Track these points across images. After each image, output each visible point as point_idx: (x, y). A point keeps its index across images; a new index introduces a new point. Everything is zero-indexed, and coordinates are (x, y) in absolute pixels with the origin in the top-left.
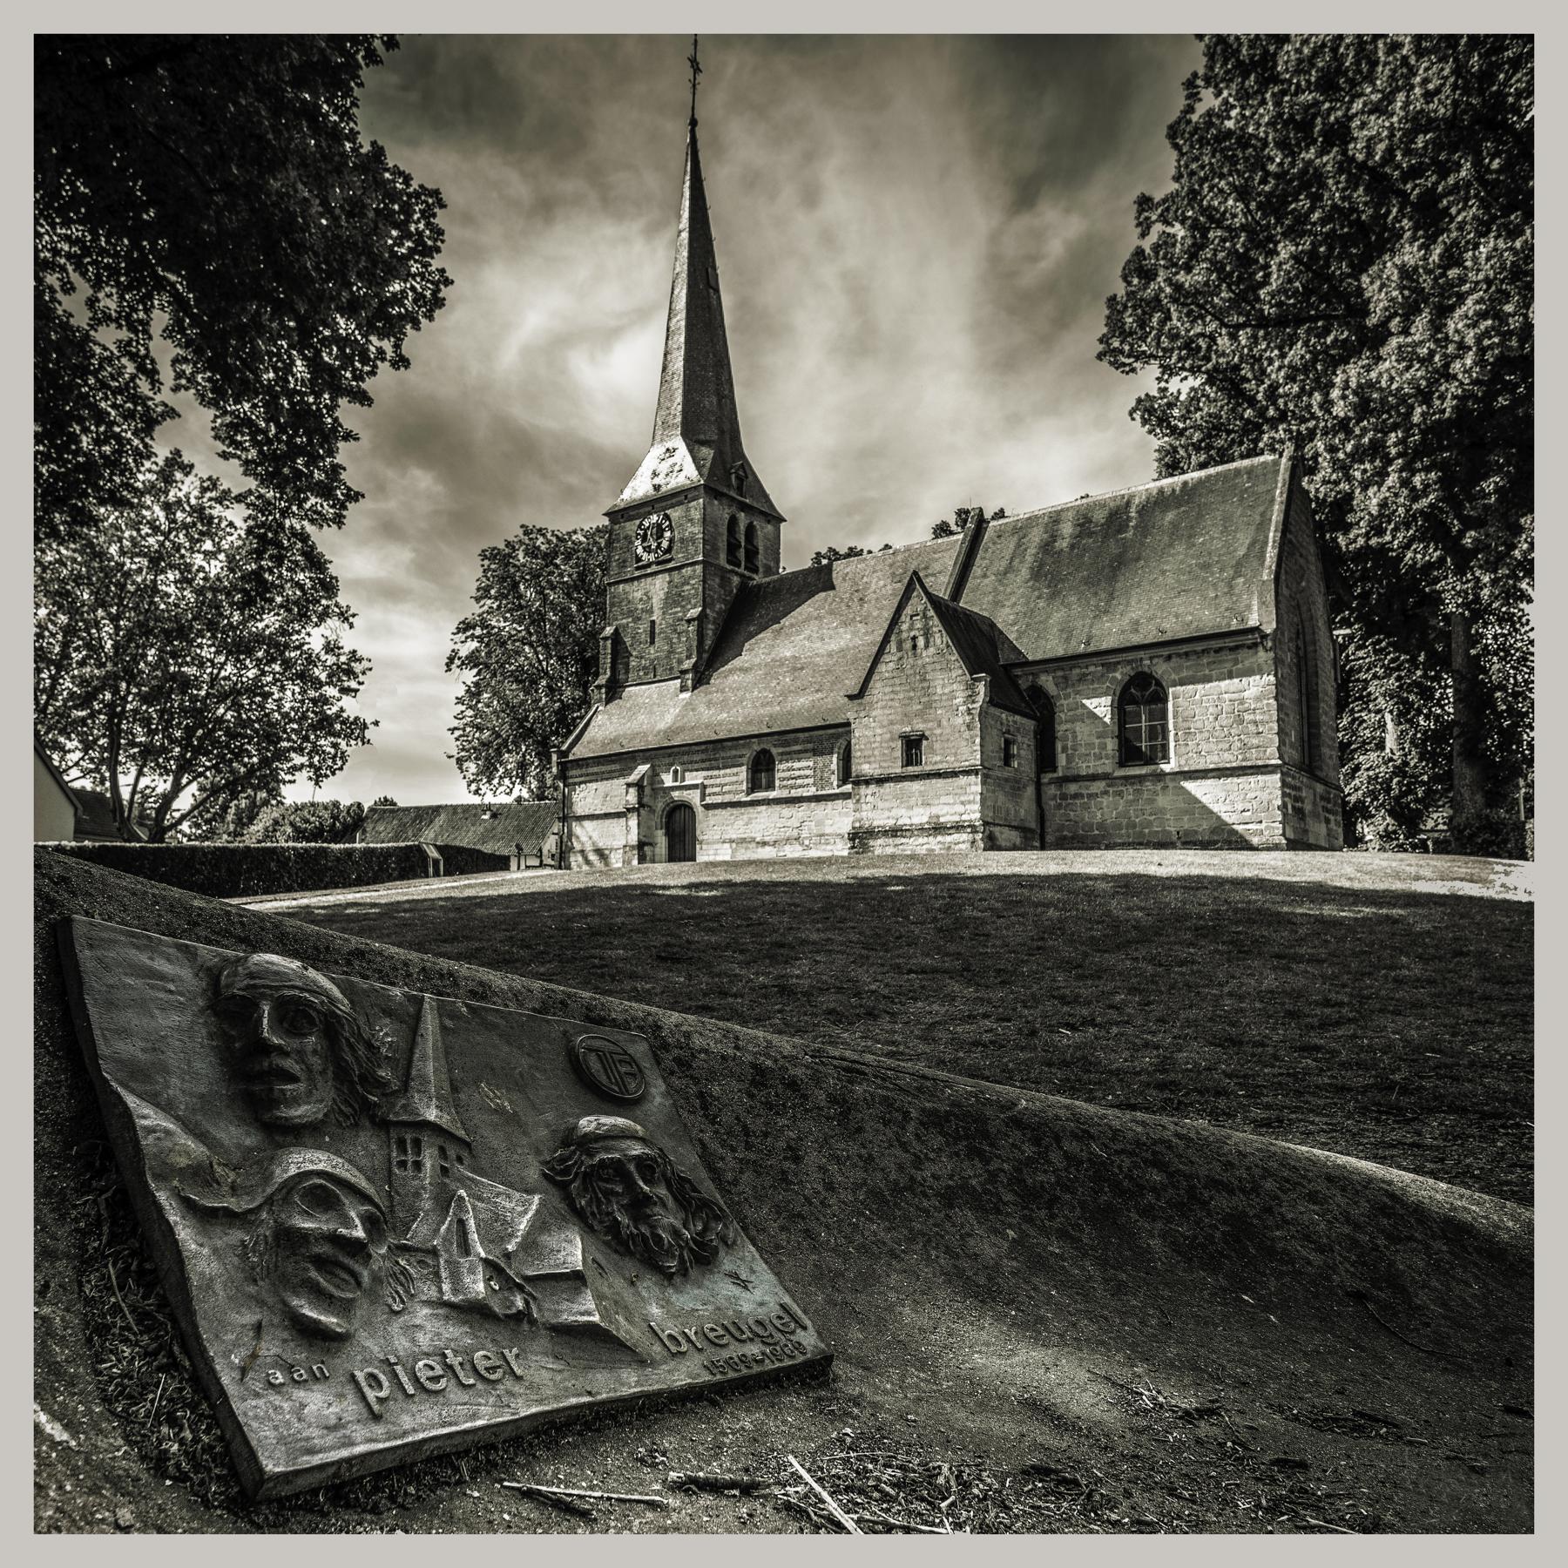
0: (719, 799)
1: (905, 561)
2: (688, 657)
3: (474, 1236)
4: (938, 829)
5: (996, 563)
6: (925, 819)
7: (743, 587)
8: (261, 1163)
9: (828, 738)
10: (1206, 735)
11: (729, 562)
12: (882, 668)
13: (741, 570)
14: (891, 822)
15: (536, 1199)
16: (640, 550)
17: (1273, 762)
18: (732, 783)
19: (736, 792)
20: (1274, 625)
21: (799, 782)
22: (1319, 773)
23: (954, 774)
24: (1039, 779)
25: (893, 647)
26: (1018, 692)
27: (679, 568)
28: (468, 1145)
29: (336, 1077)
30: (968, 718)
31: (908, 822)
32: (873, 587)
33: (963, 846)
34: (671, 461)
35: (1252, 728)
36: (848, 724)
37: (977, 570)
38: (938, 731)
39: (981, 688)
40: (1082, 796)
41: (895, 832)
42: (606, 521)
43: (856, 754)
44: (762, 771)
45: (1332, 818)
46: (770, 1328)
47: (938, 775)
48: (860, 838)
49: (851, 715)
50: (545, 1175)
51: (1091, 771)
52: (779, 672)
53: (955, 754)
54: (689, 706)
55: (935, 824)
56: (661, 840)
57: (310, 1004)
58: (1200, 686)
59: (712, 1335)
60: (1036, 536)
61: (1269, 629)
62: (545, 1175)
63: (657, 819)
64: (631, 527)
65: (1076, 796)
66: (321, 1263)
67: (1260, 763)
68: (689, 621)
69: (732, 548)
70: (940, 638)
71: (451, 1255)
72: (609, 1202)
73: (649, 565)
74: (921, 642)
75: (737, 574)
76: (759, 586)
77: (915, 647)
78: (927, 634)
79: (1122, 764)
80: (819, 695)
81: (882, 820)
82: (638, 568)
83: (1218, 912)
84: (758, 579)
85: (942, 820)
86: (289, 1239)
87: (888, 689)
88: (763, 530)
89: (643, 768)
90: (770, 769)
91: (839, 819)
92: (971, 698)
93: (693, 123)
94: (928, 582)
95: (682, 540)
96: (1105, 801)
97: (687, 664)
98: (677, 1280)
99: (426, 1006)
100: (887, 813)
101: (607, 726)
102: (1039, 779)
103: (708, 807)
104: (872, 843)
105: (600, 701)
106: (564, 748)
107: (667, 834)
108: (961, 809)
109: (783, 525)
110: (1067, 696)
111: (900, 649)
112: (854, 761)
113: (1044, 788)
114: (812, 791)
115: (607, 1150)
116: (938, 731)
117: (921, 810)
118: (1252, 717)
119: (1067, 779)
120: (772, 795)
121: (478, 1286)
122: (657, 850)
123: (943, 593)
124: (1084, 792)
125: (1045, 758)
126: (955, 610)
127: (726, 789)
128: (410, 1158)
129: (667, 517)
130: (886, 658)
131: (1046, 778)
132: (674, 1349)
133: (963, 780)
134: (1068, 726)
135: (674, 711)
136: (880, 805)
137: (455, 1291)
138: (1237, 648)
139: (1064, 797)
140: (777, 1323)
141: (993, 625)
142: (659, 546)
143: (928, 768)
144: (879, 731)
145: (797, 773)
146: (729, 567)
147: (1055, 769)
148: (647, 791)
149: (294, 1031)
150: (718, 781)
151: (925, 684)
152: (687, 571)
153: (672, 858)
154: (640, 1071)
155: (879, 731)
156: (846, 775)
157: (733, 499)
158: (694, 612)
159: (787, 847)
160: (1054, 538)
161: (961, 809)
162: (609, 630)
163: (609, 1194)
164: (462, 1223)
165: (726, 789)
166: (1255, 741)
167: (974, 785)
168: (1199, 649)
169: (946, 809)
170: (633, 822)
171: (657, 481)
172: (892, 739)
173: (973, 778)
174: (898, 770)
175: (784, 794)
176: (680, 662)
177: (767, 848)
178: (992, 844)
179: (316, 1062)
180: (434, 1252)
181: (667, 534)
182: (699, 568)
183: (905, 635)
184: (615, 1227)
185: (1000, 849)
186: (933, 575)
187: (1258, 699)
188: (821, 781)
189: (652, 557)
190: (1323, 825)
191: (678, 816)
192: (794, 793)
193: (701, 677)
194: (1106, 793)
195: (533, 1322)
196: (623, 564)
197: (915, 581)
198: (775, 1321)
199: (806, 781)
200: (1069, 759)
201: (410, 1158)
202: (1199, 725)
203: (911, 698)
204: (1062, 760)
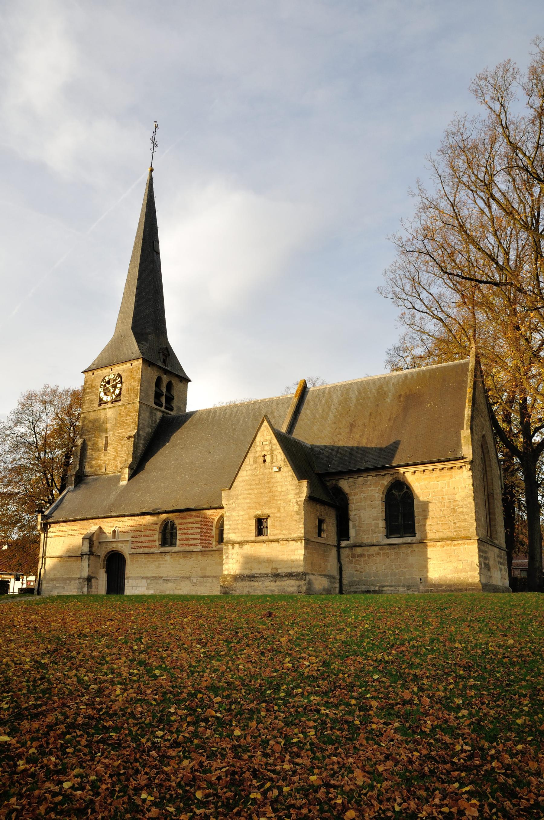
7: (163, 419)
20: (471, 457)
21: (192, 542)
22: (496, 542)
24: (339, 544)
38: (278, 515)
45: (502, 567)
47: (277, 541)
58: (506, 567)
60: (337, 398)
63: (101, 561)
65: (361, 556)
69: (158, 395)
70: (280, 455)
74: (268, 459)
75: (160, 410)
77: (264, 461)
78: (272, 451)
79: (388, 536)
87: (247, 487)
88: (177, 385)
90: (173, 535)
92: (299, 494)
93: (152, 170)
96: (378, 559)
102: (339, 544)
107: (107, 572)
109: (189, 383)
110: (356, 494)
111: (255, 461)
112: (225, 532)
113: (342, 551)
114: (199, 548)
116: (278, 515)
118: (461, 510)
119: (355, 546)
123: (284, 429)
124: (366, 553)
125: (343, 532)
126: (290, 439)
131: (344, 544)
139: (354, 556)
143: (271, 538)
145: (190, 536)
146: (155, 407)
147: (348, 539)
148: (96, 543)
151: (271, 485)
170: (85, 563)
174: (253, 538)
175: (182, 549)
177: (170, 584)
187: (463, 500)
190: (499, 572)
192: (188, 548)
194: (378, 554)
200: (357, 534)
204: (352, 533)
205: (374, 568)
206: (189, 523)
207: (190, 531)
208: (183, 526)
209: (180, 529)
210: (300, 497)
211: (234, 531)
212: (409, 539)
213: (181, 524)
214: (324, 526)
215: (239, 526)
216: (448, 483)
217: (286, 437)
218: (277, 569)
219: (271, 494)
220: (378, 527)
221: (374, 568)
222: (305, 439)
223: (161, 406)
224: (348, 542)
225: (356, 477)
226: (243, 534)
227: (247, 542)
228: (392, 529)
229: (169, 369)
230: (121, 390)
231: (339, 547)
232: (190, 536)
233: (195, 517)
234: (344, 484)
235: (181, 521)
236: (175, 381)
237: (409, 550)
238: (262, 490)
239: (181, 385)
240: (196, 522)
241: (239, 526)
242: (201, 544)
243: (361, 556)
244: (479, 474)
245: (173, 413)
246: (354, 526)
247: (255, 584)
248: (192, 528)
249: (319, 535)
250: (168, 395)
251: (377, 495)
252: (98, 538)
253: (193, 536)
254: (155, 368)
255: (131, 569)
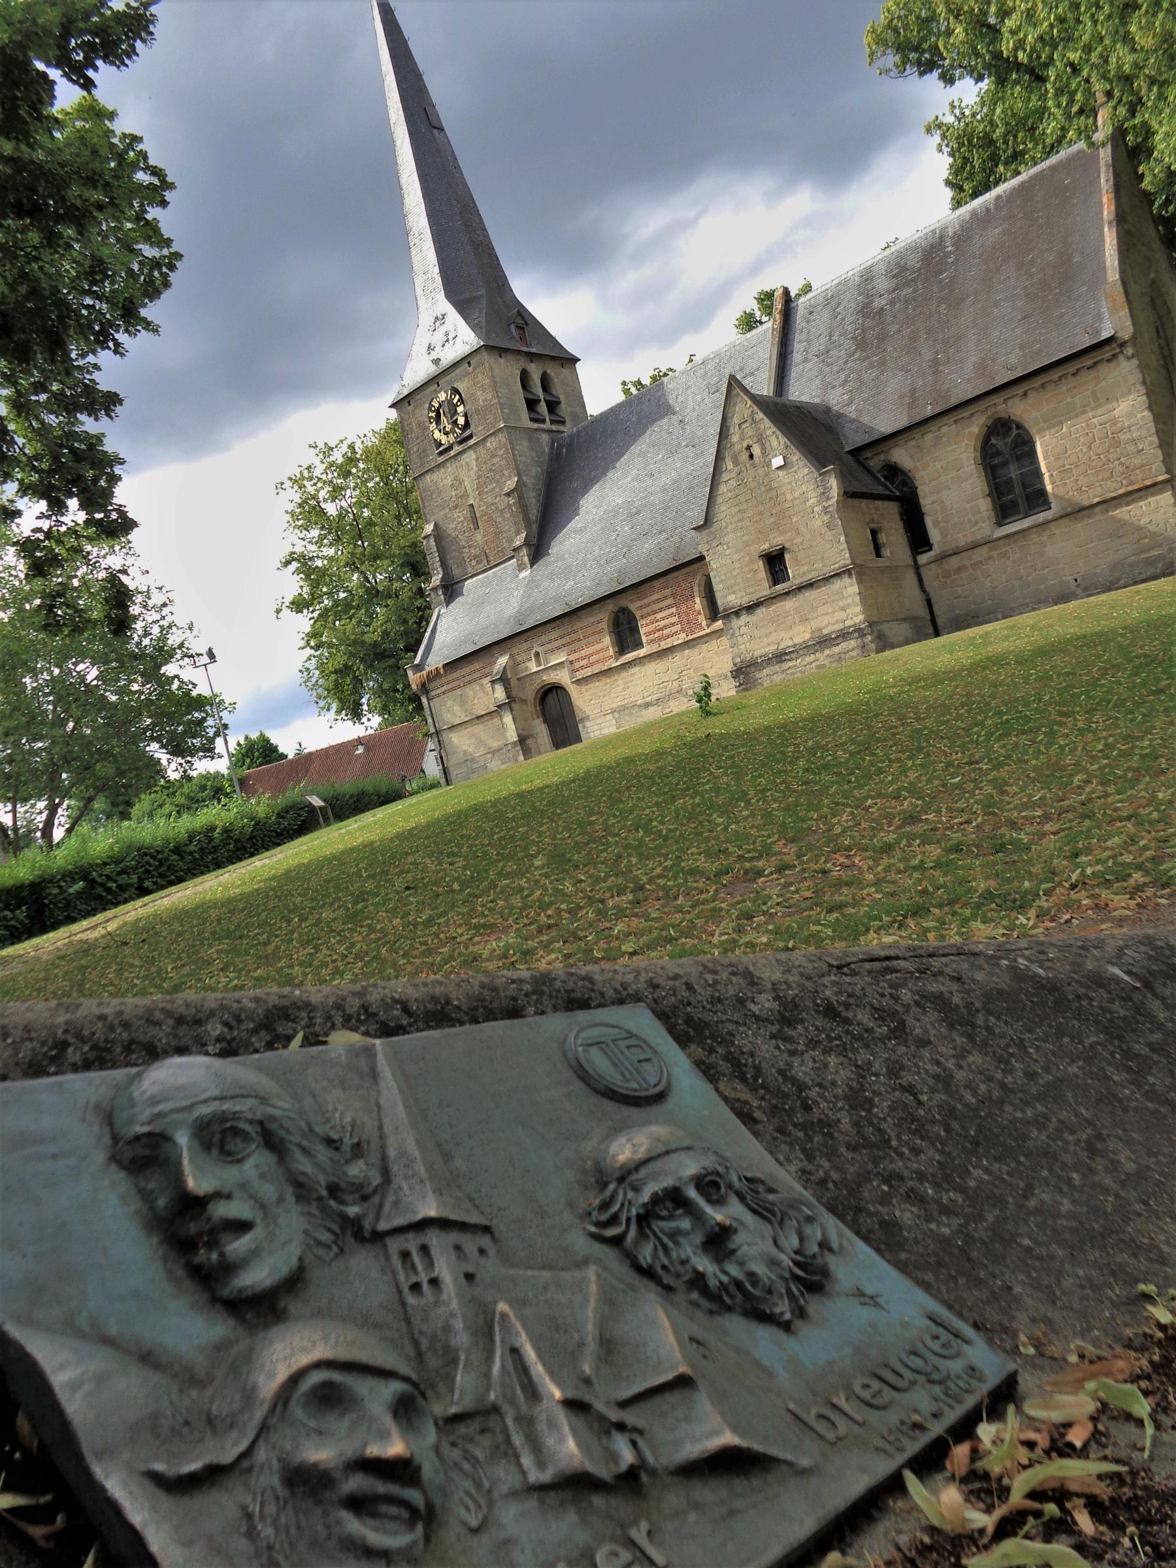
0: (588, 672)
1: (718, 367)
2: (518, 533)
3: (538, 1369)
4: (823, 642)
5: (815, 344)
6: (807, 636)
8: (237, 1365)
9: (686, 573)
10: (1083, 468)
11: (532, 420)
12: (723, 488)
13: (547, 425)
14: (773, 648)
15: (591, 1273)
16: (437, 435)
17: (1161, 478)
18: (598, 652)
19: (605, 660)
20: (1131, 329)
23: (827, 580)
24: (915, 561)
25: (729, 464)
26: (875, 478)
27: (484, 440)
28: (487, 1229)
29: (299, 1198)
30: (826, 518)
31: (790, 643)
32: (691, 404)
33: (854, 653)
34: (442, 330)
35: (1131, 448)
36: (702, 558)
37: (797, 356)
38: (799, 540)
39: (833, 483)
40: (965, 568)
41: (780, 657)
42: (393, 414)
43: (717, 587)
44: (625, 634)
46: (929, 1355)
47: (810, 585)
48: (743, 673)
49: (703, 549)
50: (593, 1236)
51: (969, 539)
52: (611, 526)
53: (822, 559)
54: (531, 583)
55: (814, 638)
56: (541, 730)
57: (235, 1116)
59: (866, 1395)
61: (1126, 332)
62: (593, 1236)
63: (531, 708)
64: (423, 413)
65: (959, 570)
66: (358, 1504)
67: (1148, 483)
68: (508, 494)
69: (531, 404)
70: (777, 440)
71: (518, 1409)
72: (677, 1243)
73: (450, 448)
74: (756, 450)
76: (571, 437)
77: (751, 456)
78: (761, 439)
79: (1000, 524)
80: (664, 536)
81: (763, 648)
82: (441, 453)
83: (106, 599)
84: (567, 429)
85: (825, 632)
86: (305, 1482)
87: (735, 510)
88: (558, 375)
89: (503, 661)
90: (635, 630)
91: (716, 660)
92: (825, 495)
94: (747, 383)
95: (477, 411)
97: (519, 540)
98: (798, 1323)
99: (380, 1057)
100: (766, 641)
101: (451, 630)
102: (915, 561)
103: (578, 682)
104: (758, 675)
105: (439, 604)
106: (417, 661)
107: (545, 721)
108: (843, 615)
109: (578, 365)
111: (736, 463)
113: (923, 571)
114: (682, 638)
115: (654, 1176)
116: (799, 540)
117: (801, 628)
118: (1128, 436)
119: (944, 557)
120: (642, 652)
121: (568, 1448)
122: (540, 740)
125: (919, 540)
126: (785, 406)
127: (593, 659)
128: (424, 1278)
129: (456, 391)
130: (725, 477)
131: (923, 559)
132: (831, 1436)
133: (837, 584)
134: (934, 498)
135: (518, 594)
136: (756, 633)
137: (541, 1465)
138: (1095, 364)
139: (947, 574)
140: (936, 1346)
141: (827, 410)
142: (455, 423)
144: (736, 557)
145: (662, 623)
146: (535, 426)
148: (513, 682)
149: (229, 1156)
150: (583, 653)
151: (773, 493)
152: (491, 444)
153: (558, 744)
154: (655, 1052)
155: (736, 557)
156: (714, 612)
157: (519, 352)
158: (511, 483)
159: (671, 703)
160: (870, 298)
161: (843, 615)
162: (429, 528)
163: (674, 1235)
164: (515, 1351)
165: (593, 659)
166: (1137, 461)
167: (850, 588)
168: (1089, 363)
169: (826, 619)
170: (508, 719)
171: (434, 355)
172: (752, 561)
173: (846, 580)
174: (767, 592)
175: (655, 648)
176: (511, 541)
177: (652, 709)
178: (884, 643)
179: (268, 1191)
180: (495, 1409)
181: (460, 409)
182: (502, 437)
183: (737, 447)
184: (698, 1281)
185: (892, 646)
186: (752, 374)
187: (1130, 415)
188: (689, 624)
189: (452, 438)
191: (551, 698)
192: (664, 645)
193: (537, 549)
194: (990, 558)
195: (653, 1473)
196: (423, 454)
197: (734, 384)
198: (929, 1343)
199: (673, 629)
201: (424, 1278)
202: (1073, 459)
203: (761, 513)
204: (934, 535)
205: (988, 584)
206: (654, 602)
207: (659, 616)
208: (645, 611)
209: (642, 617)
210: (828, 499)
211: (731, 589)
212: (1042, 517)
213: (641, 607)
214: (882, 538)
215: (739, 580)
216: (1094, 394)
217: (776, 404)
218: (820, 630)
219: (777, 509)
220: (978, 512)
221: (988, 584)
222: (936, 523)
223: (543, 421)
224: (931, 554)
225: (918, 436)
226: (750, 590)
227: (758, 604)
228: (1004, 511)
229: (534, 350)
230: (466, 415)
231: (917, 567)
232: (662, 623)
233: (660, 589)
234: (901, 456)
235: (639, 603)
236: (552, 370)
237: (1045, 537)
238: (761, 508)
239: (565, 372)
240: (665, 598)
241: (739, 580)
242: (683, 630)
243: (959, 570)
244: (1154, 361)
245: (567, 429)
246: (936, 523)
247: (790, 664)
248: (661, 610)
249: (878, 555)
250: (549, 398)
251: (964, 456)
252: (515, 673)
253: (667, 622)
254: (511, 357)
255: (583, 700)
